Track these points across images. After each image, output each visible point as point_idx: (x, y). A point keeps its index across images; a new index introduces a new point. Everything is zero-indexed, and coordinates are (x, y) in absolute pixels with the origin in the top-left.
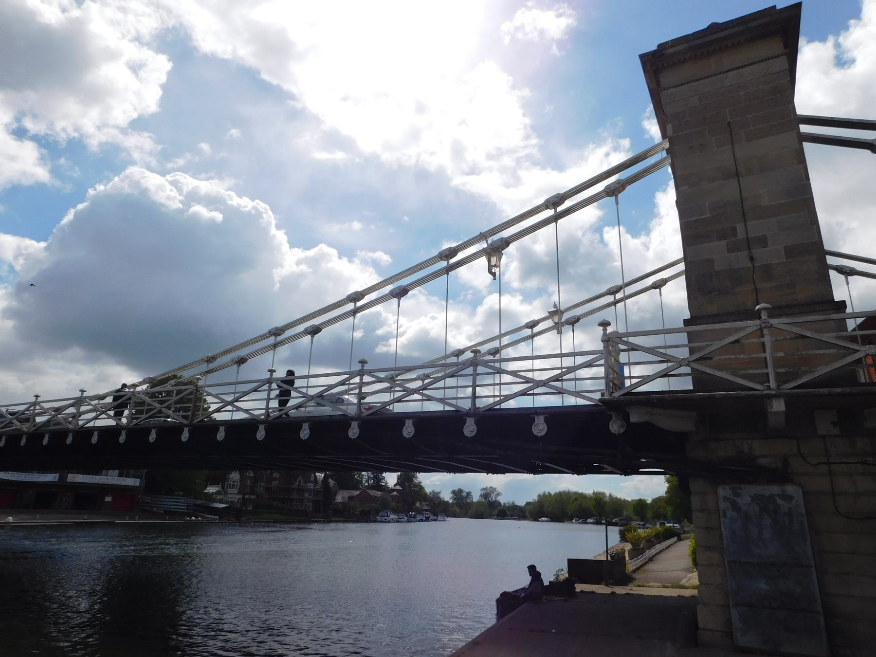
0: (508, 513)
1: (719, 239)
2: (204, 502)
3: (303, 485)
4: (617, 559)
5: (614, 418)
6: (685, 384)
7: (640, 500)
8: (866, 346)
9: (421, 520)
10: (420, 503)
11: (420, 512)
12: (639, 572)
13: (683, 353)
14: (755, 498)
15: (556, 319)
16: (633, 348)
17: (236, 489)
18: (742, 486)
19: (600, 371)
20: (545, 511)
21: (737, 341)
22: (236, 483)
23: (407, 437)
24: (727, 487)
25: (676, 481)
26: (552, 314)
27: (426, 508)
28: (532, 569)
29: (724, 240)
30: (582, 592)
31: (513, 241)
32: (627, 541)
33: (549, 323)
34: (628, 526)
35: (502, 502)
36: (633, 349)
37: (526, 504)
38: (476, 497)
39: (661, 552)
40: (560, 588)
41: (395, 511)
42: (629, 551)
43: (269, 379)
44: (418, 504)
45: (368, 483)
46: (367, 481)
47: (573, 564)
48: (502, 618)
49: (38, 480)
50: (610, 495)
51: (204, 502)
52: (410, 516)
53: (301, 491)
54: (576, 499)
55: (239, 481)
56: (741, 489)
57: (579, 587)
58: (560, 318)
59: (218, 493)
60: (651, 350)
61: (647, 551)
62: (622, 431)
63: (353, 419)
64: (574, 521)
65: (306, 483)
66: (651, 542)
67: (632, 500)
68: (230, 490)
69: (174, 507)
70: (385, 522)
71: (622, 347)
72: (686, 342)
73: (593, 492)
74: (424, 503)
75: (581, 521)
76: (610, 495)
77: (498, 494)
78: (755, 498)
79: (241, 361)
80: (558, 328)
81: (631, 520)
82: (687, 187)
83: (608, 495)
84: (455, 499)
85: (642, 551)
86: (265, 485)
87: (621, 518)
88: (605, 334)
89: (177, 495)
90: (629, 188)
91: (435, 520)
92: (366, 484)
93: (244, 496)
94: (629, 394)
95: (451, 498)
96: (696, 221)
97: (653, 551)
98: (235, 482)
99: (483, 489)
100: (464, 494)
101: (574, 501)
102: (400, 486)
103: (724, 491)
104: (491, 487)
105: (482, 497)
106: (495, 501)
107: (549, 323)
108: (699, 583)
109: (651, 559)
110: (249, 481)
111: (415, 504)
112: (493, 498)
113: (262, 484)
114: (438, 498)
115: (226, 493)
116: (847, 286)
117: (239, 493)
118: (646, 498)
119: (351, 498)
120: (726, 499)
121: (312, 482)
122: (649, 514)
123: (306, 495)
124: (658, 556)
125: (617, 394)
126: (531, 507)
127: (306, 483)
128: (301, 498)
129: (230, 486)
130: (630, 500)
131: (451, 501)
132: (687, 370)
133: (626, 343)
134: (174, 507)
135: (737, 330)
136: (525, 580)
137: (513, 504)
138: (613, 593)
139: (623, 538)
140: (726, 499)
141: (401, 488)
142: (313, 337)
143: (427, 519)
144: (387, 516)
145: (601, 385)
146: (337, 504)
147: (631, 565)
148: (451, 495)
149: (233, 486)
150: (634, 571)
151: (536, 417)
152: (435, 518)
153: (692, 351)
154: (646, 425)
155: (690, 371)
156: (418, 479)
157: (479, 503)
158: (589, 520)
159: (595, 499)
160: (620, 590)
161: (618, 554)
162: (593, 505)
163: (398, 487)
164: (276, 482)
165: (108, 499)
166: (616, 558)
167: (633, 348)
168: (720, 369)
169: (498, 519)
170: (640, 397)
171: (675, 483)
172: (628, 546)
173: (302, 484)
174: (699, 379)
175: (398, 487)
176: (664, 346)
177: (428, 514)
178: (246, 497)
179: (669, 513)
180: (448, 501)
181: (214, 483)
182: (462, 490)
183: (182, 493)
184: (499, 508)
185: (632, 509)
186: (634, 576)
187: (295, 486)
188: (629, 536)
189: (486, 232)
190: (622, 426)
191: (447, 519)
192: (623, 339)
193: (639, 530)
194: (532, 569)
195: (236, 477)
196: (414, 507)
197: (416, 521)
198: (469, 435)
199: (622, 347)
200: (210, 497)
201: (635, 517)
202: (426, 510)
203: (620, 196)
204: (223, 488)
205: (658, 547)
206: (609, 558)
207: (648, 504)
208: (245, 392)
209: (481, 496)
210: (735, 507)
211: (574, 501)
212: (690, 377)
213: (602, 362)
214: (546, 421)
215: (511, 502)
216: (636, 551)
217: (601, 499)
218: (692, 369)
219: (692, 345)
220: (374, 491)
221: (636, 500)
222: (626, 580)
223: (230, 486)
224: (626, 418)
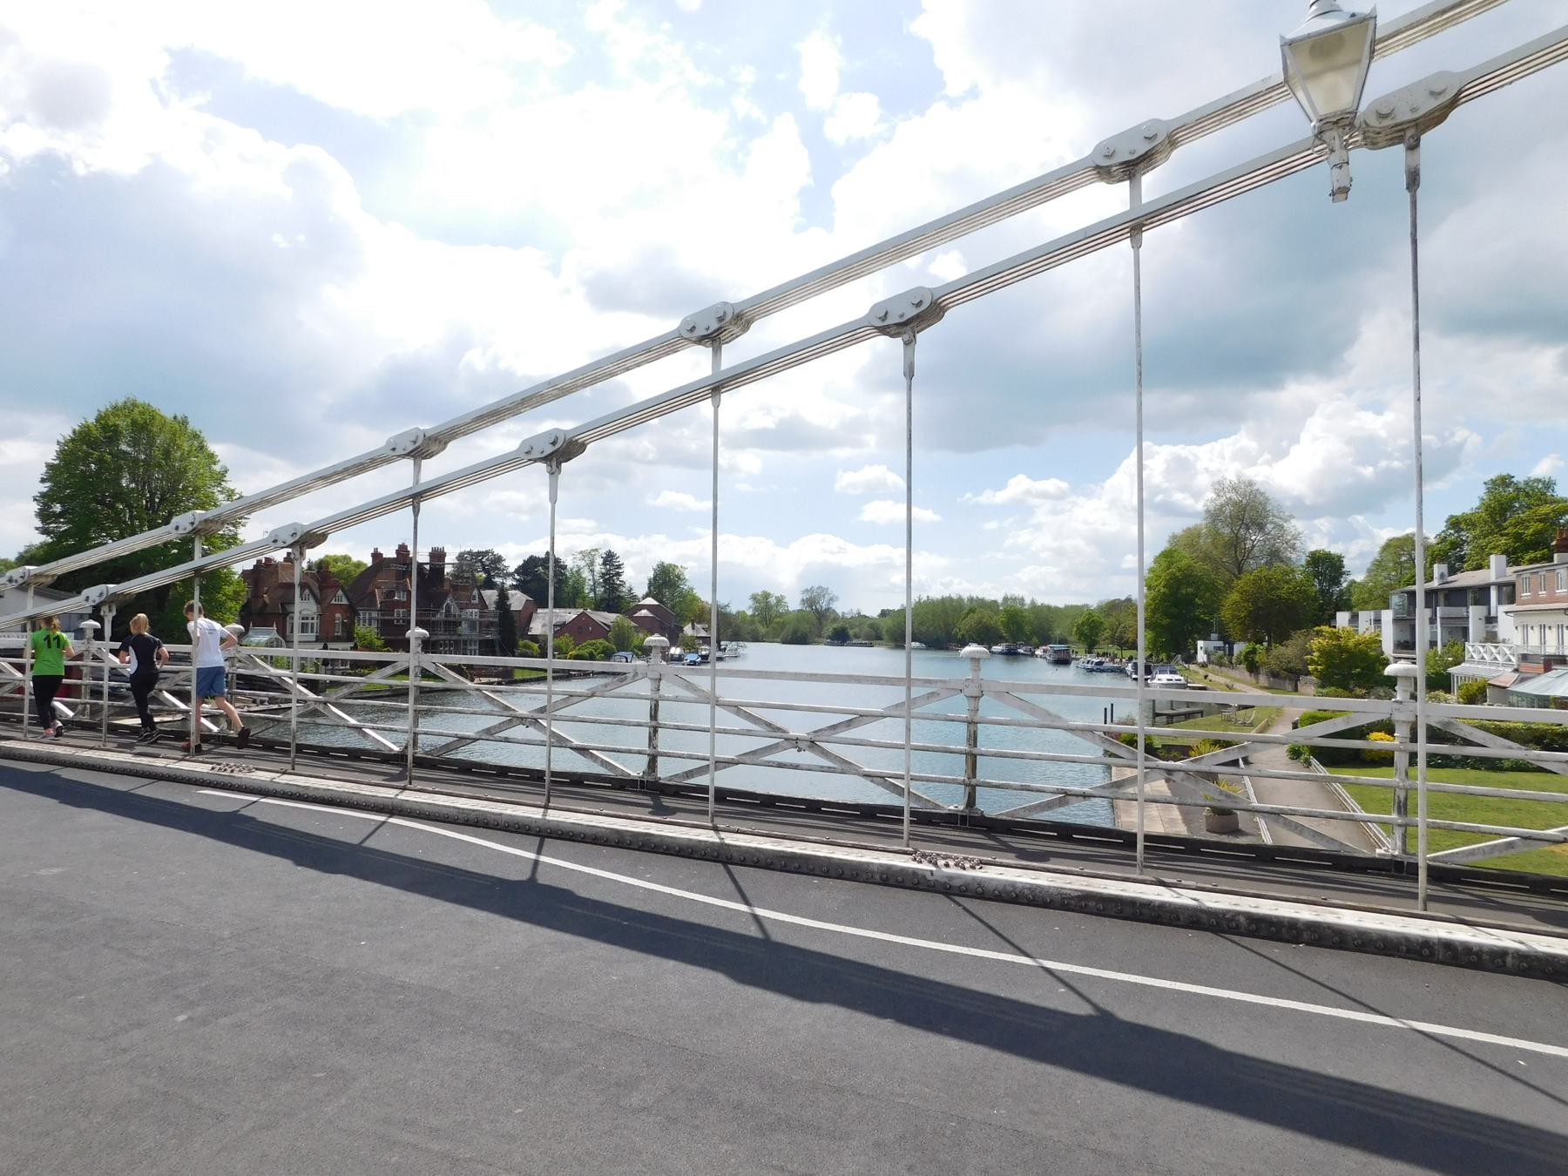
0: (851, 632)
8: (31, 683)
17: (312, 632)
22: (310, 621)
25: (1164, 587)
35: (839, 611)
38: (794, 604)
45: (595, 593)
46: (593, 590)
50: (1033, 602)
54: (972, 611)
55: (315, 616)
65: (461, 609)
74: (699, 626)
76: (1033, 602)
77: (831, 599)
79: (562, 452)
86: (380, 617)
92: (592, 595)
95: (750, 607)
98: (307, 618)
99: (807, 591)
100: (773, 601)
101: (968, 613)
102: (653, 598)
104: (820, 587)
105: (804, 604)
106: (828, 609)
110: (338, 615)
111: (681, 630)
112: (823, 604)
113: (374, 614)
116: (1408, 195)
121: (474, 606)
127: (461, 609)
129: (312, 628)
131: (749, 613)
137: (859, 613)
141: (656, 603)
148: (751, 603)
156: (688, 583)
162: (1002, 622)
163: (650, 601)
164: (401, 611)
171: (1163, 590)
173: (454, 610)
175: (650, 601)
176: (964, 818)
180: (744, 612)
182: (769, 594)
184: (835, 626)
195: (308, 610)
196: (680, 635)
211: (968, 613)
215: (855, 611)
220: (602, 613)
223: (312, 628)
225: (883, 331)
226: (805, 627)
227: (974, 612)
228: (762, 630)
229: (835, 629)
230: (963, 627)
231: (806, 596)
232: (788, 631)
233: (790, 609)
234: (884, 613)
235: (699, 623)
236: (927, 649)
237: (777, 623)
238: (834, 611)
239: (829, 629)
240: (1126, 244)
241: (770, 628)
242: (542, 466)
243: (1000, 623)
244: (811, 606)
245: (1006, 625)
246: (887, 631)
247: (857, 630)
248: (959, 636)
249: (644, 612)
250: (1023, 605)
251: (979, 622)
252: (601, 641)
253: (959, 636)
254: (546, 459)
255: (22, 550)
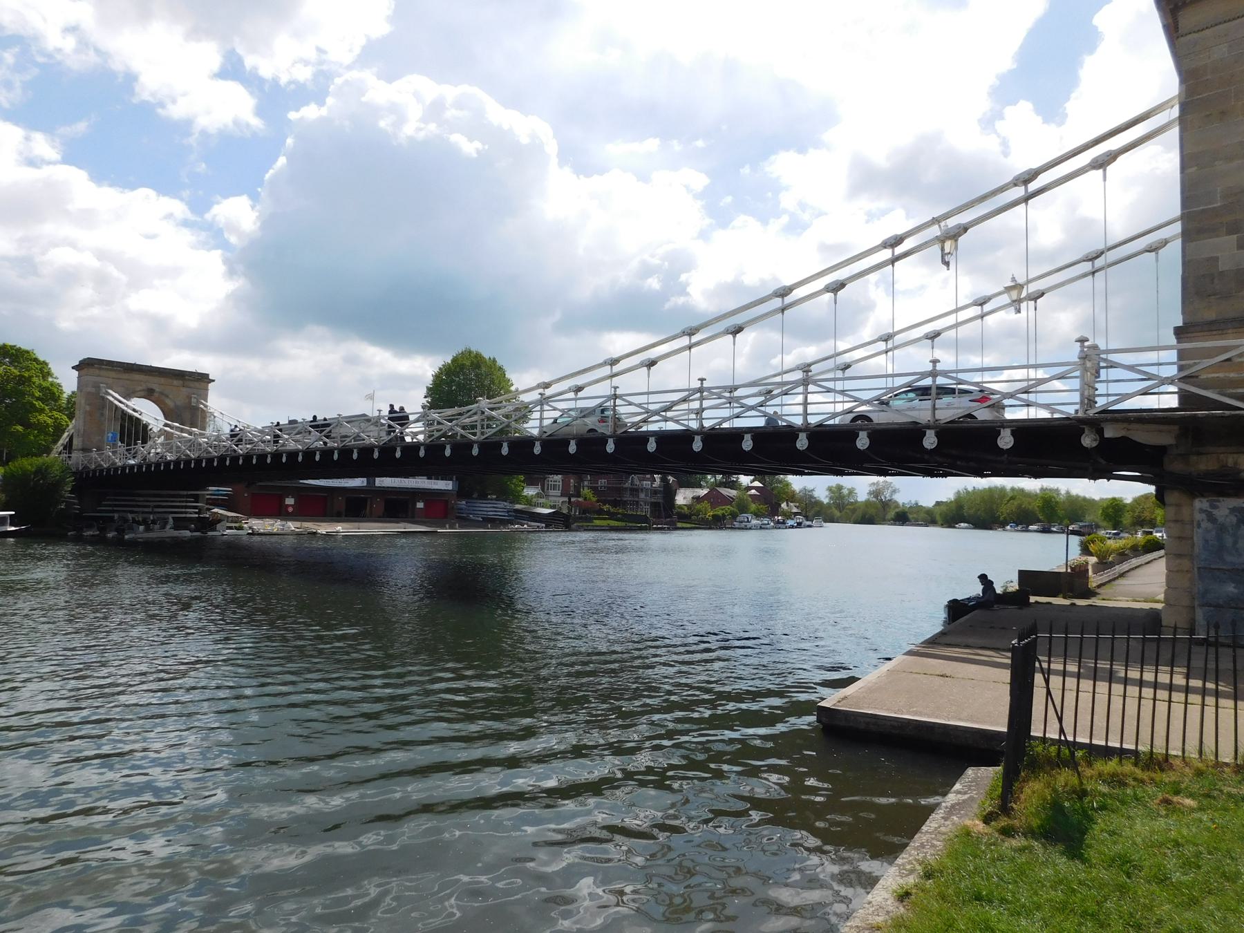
0: (910, 516)
1: (1230, 232)
2: (524, 506)
3: (638, 483)
4: (1079, 573)
5: (1086, 431)
6: (1172, 401)
7: (1114, 499)
9: (792, 527)
10: (787, 503)
11: (789, 515)
12: (1104, 587)
13: (1172, 371)
14: (1233, 510)
15: (1014, 294)
16: (1113, 365)
18: (1221, 499)
19: (1076, 384)
20: (965, 514)
21: (1229, 360)
23: (862, 448)
24: (1204, 500)
26: (1008, 289)
27: (795, 510)
28: (983, 578)
29: (1233, 234)
30: (1037, 602)
31: (972, 226)
32: (1091, 554)
33: (1005, 299)
34: (1092, 536)
36: (1111, 367)
37: (935, 505)
39: (1136, 567)
40: (1016, 599)
41: (757, 515)
42: (1093, 566)
43: (699, 388)
44: (784, 505)
47: (1024, 576)
48: (953, 622)
49: (346, 485)
50: (1068, 492)
51: (524, 506)
52: (778, 522)
53: (635, 491)
54: (1013, 498)
56: (1219, 501)
57: (1033, 599)
58: (1020, 293)
59: (538, 495)
60: (1131, 368)
61: (1117, 566)
62: (1095, 444)
63: (800, 430)
64: (1008, 527)
66: (1123, 556)
67: (1102, 500)
68: (552, 492)
69: (491, 513)
70: (746, 528)
71: (1102, 364)
72: (1175, 359)
73: (1040, 487)
75: (1019, 528)
76: (1068, 492)
77: (894, 491)
78: (1233, 510)
79: (651, 364)
80: (1016, 304)
81: (1098, 527)
82: (1196, 168)
83: (1063, 492)
84: (831, 498)
85: (1112, 565)
87: (1081, 524)
88: (1082, 351)
89: (489, 499)
90: (1121, 159)
91: (810, 526)
93: (570, 499)
94: (1104, 411)
95: (827, 497)
96: (1203, 211)
97: (1125, 567)
100: (845, 492)
101: (1008, 501)
103: (1200, 504)
107: (1005, 299)
108: (658, 139)
109: (1122, 575)
110: (572, 481)
111: (780, 505)
114: (812, 497)
115: (548, 496)
116: (1002, 289)
117: (562, 495)
118: (1123, 496)
119: (697, 499)
120: (1202, 511)
122: (1127, 519)
123: (642, 496)
124: (1132, 573)
125: (1091, 413)
126: (944, 508)
128: (637, 499)
130: (1097, 498)
132: (1174, 389)
133: (1105, 360)
134: (491, 513)
135: (1226, 349)
136: (977, 589)
137: (917, 504)
138: (1073, 604)
139: (1085, 550)
140: (1202, 511)
141: (761, 485)
142: (734, 337)
143: (799, 525)
144: (748, 521)
145: (1076, 397)
146: (680, 507)
147: (1094, 580)
148: (827, 493)
149: (554, 487)
150: (1099, 586)
151: (1002, 430)
152: (809, 523)
153: (1181, 368)
154: (1124, 440)
155: (1176, 390)
157: (867, 503)
158: (1031, 527)
159: (1042, 498)
160: (1081, 602)
161: (1080, 566)
162: (1038, 506)
165: (420, 505)
166: (1077, 570)
167: (1113, 365)
168: (1205, 388)
169: (895, 525)
170: (1116, 415)
172: (1093, 560)
174: (1184, 397)
177: (800, 518)
178: (573, 499)
179: (1159, 518)
181: (531, 483)
183: (495, 497)
184: (897, 510)
185: (1101, 512)
186: (1098, 591)
187: (627, 485)
188: (1092, 547)
189: (939, 217)
190: (1096, 440)
191: (824, 524)
192: (1102, 356)
193: (1109, 541)
194: (983, 578)
197: (786, 528)
198: (929, 448)
199: (1102, 364)
200: (529, 501)
201: (1104, 524)
202: (796, 514)
203: (1109, 168)
204: (543, 489)
205: (1135, 562)
206: (1069, 570)
207: (1125, 505)
208: (673, 402)
209: (870, 493)
210: (1211, 518)
211: (1008, 501)
212: (1176, 396)
213: (1077, 373)
214: (1013, 433)
215: (913, 502)
216: (1103, 565)
217: (1051, 497)
218: (1180, 389)
219: (1183, 363)
221: (1106, 499)
222: (1089, 593)
224: (1100, 432)
225: (777, 297)
226: (872, 511)
227: (1014, 499)
228: (837, 513)
229: (897, 513)
230: (1004, 510)
231: (874, 488)
232: (859, 514)
233: (859, 500)
234: (938, 503)
235: (792, 502)
236: (974, 528)
237: (849, 509)
238: (896, 502)
239: (891, 514)
240: (1024, 205)
241: (843, 513)
242: (645, 368)
243: (1037, 508)
244: (876, 497)
245: (1042, 509)
246: (940, 514)
247: (915, 516)
248: (1001, 519)
249: (753, 492)
250: (1058, 494)
251: (1019, 506)
252: (729, 507)
253: (1001, 519)
254: (647, 366)
255: (487, 354)
